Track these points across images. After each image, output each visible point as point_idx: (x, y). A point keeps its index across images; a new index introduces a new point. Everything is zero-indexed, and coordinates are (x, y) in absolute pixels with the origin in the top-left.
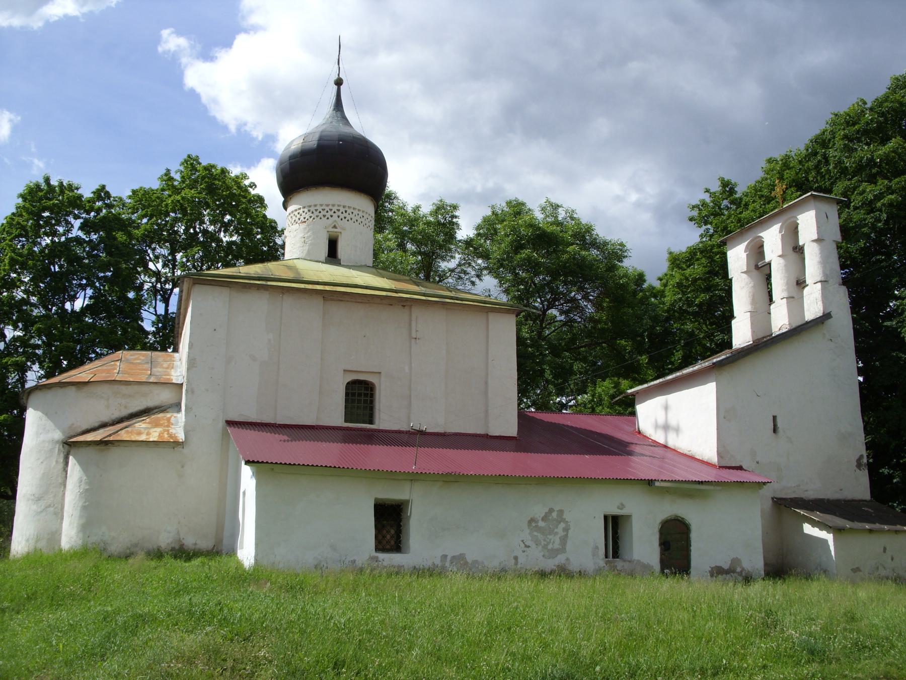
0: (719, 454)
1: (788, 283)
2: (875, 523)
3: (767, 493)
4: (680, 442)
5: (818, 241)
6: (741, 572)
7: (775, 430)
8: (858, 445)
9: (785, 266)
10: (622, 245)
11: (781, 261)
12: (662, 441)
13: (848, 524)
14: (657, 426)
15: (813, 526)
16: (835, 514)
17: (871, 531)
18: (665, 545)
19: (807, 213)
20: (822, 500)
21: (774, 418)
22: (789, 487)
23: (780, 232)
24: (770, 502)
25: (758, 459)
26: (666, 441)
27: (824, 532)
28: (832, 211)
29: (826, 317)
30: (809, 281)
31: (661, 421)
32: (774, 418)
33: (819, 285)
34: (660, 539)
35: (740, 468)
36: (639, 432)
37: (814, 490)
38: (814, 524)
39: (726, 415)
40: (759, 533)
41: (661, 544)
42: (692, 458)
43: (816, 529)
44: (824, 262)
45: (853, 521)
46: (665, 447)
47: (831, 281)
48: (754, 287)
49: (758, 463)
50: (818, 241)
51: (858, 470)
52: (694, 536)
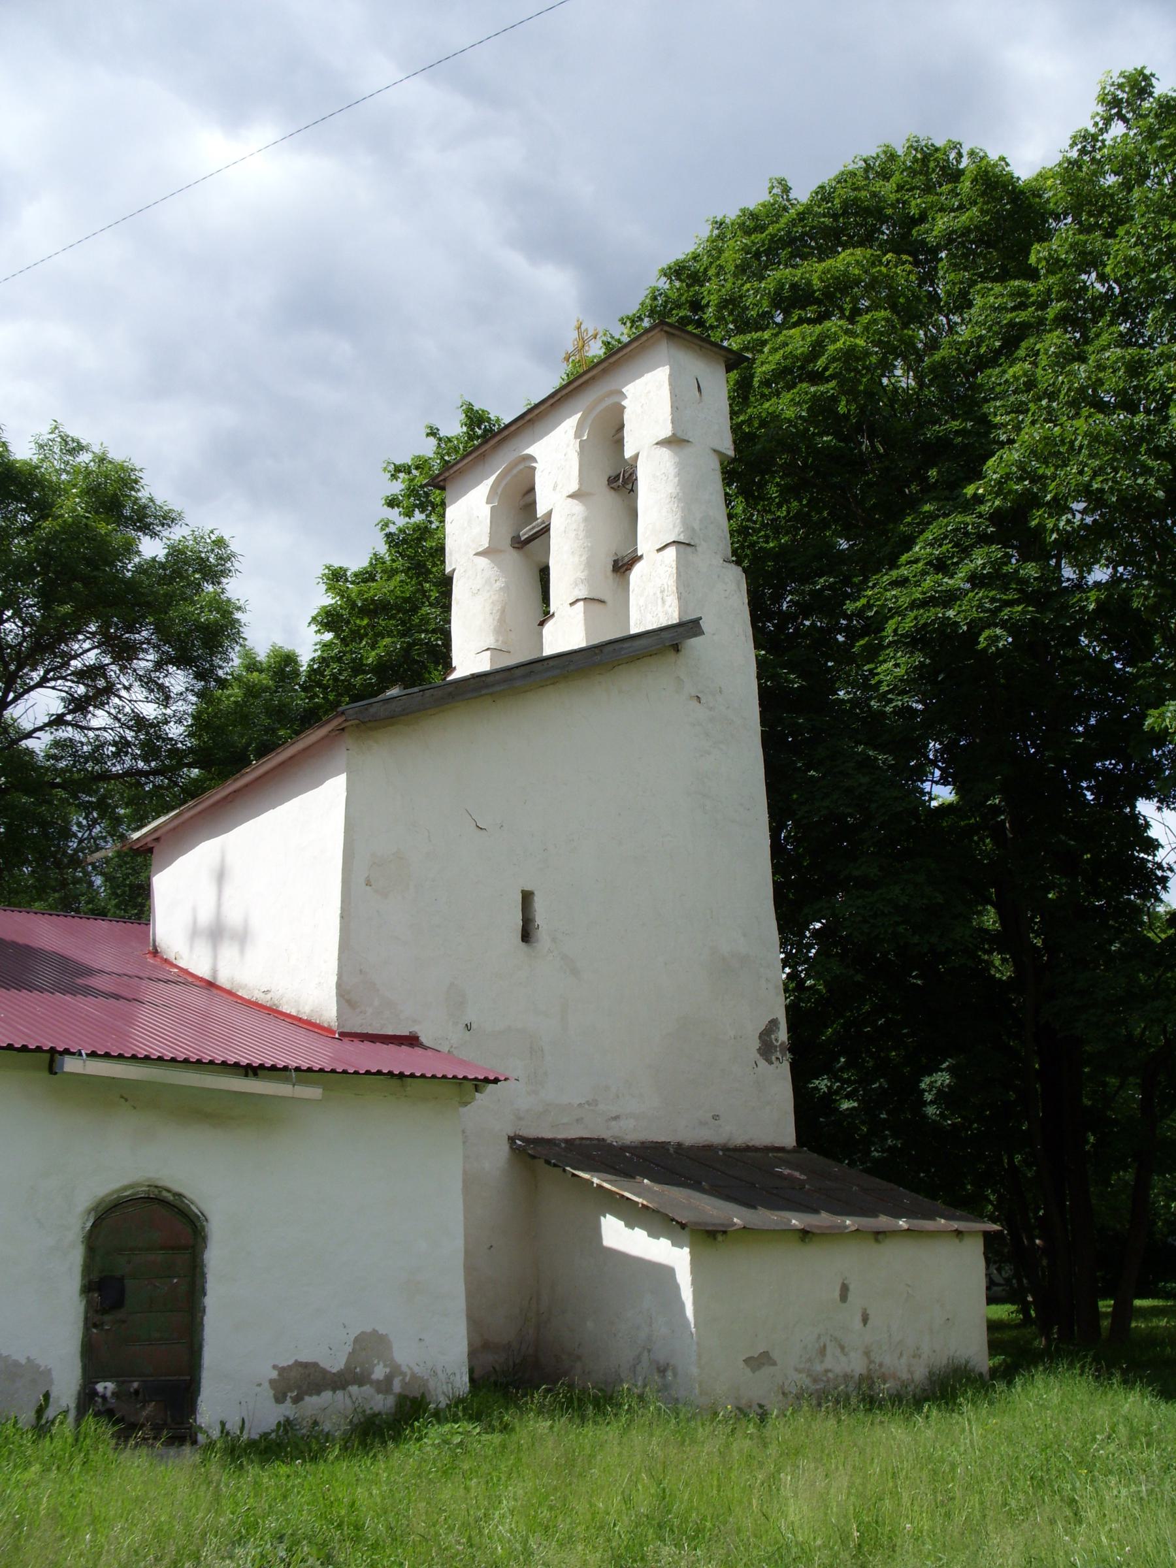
0: (344, 994)
1: (589, 564)
2: (816, 1211)
3: (495, 1117)
4: (248, 972)
5: (674, 442)
6: (389, 1379)
7: (526, 935)
8: (761, 990)
9: (586, 519)
10: (220, 543)
11: (577, 507)
12: (202, 969)
13: (738, 1216)
14: (195, 933)
15: (630, 1225)
16: (696, 1186)
17: (805, 1235)
18: (104, 1290)
19: (648, 377)
20: (659, 1148)
21: (527, 898)
22: (563, 1104)
23: (578, 435)
24: (506, 1147)
25: (471, 1016)
26: (215, 971)
27: (664, 1243)
28: (718, 385)
29: (689, 628)
30: (646, 544)
31: (205, 917)
32: (527, 898)
33: (672, 552)
34: (87, 1269)
35: (412, 1041)
36: (155, 952)
37: (635, 1119)
38: (634, 1215)
39: (368, 877)
40: (454, 1247)
41: (87, 1289)
42: (272, 1012)
43: (640, 1234)
44: (687, 496)
45: (753, 1206)
46: (211, 985)
47: (703, 547)
48: (506, 589)
49: (468, 1027)
50: (674, 442)
51: (762, 1063)
52: (215, 1258)
